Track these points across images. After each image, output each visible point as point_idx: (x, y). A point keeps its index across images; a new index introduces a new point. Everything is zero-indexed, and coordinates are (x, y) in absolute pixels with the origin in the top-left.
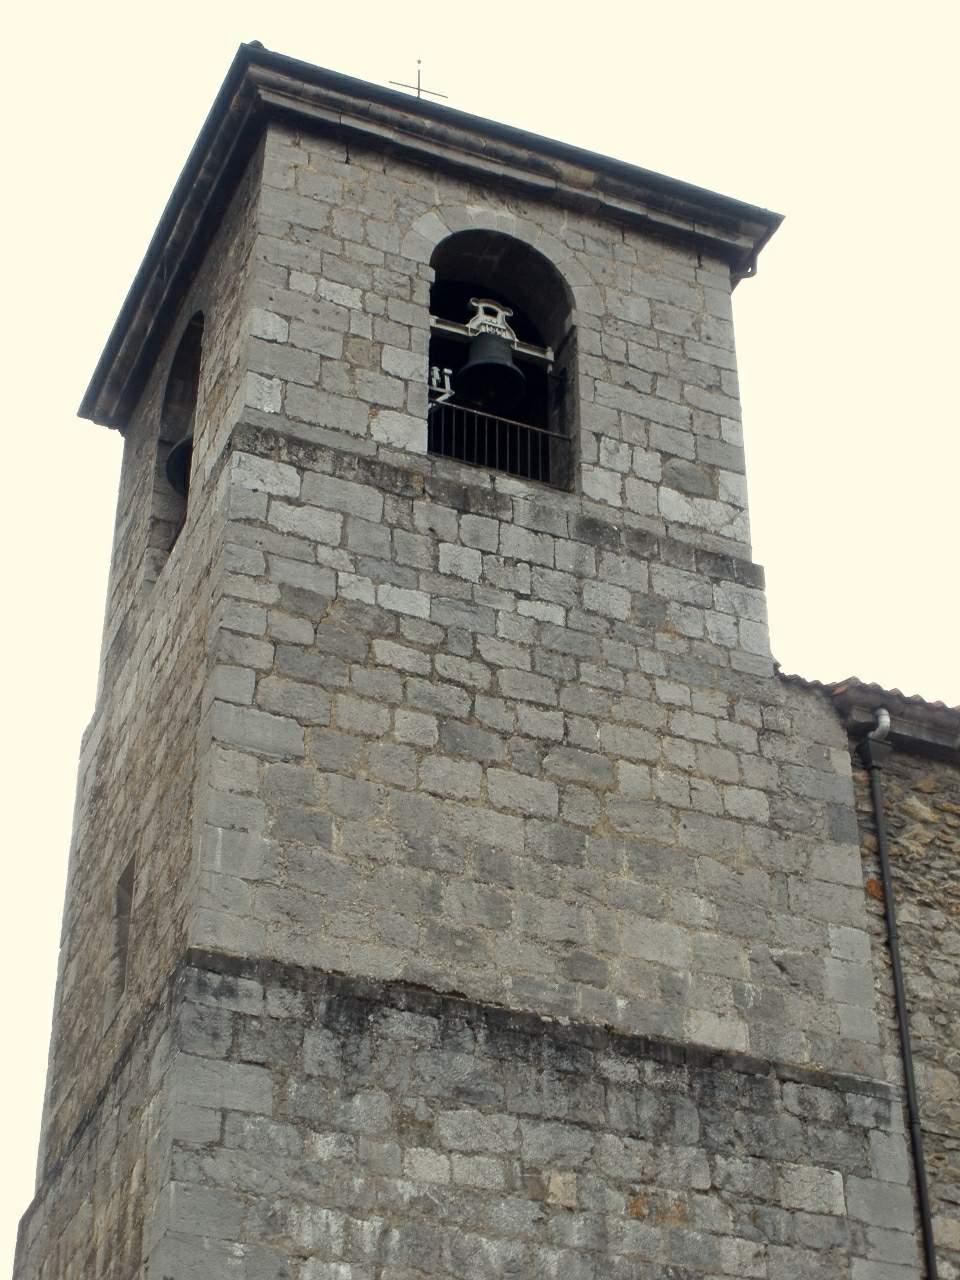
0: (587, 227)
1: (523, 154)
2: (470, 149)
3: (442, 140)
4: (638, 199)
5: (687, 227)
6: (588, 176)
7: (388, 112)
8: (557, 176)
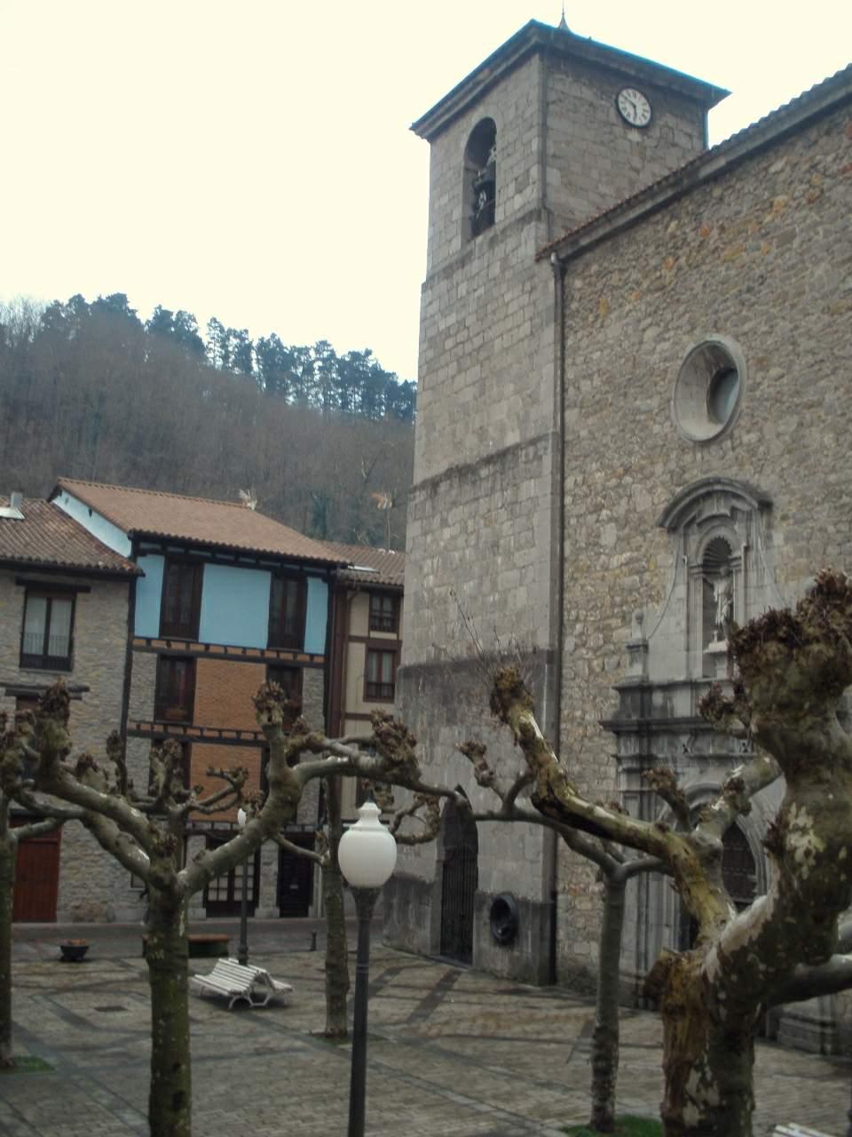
0: (502, 86)
1: (462, 93)
2: (462, 98)
3: (456, 104)
4: (503, 61)
5: (517, 56)
6: (486, 71)
7: (455, 98)
8: (482, 81)
